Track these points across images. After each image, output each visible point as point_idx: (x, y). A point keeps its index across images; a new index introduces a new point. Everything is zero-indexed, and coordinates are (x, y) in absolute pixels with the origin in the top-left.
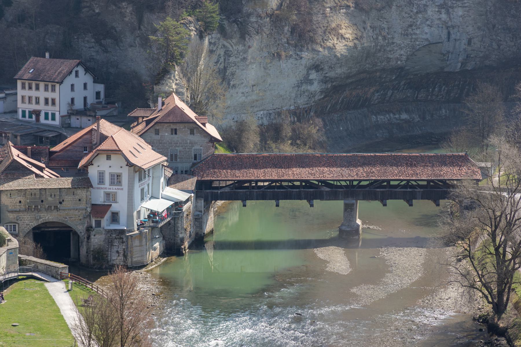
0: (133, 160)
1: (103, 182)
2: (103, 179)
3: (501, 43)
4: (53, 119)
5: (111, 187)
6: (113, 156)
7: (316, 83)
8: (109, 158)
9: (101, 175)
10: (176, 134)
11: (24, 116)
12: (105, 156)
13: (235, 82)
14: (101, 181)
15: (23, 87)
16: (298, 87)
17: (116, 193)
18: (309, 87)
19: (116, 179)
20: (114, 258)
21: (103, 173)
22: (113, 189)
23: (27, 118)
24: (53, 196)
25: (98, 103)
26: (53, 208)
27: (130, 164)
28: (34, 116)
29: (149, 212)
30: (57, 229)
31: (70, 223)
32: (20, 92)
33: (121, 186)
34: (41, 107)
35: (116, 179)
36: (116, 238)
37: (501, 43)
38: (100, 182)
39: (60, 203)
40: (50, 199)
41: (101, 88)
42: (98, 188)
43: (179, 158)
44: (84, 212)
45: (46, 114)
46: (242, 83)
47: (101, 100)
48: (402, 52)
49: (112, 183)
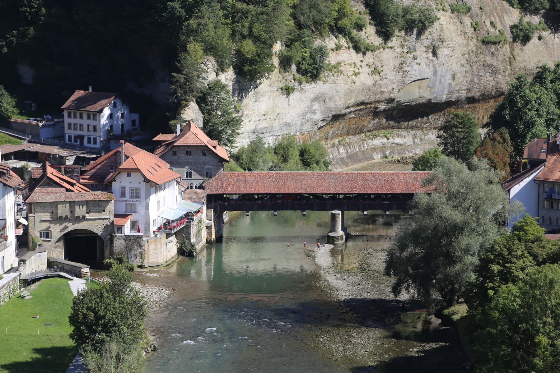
0: (149, 176)
1: (124, 196)
3: (482, 78)
4: (95, 142)
5: (131, 200)
6: (133, 174)
7: (318, 113)
8: (129, 175)
9: (123, 190)
10: (191, 154)
11: (70, 140)
12: (126, 174)
13: (248, 112)
15: (69, 116)
16: (303, 116)
17: (135, 204)
18: (312, 116)
23: (73, 142)
25: (134, 130)
27: (147, 181)
28: (78, 141)
29: (166, 220)
30: (85, 235)
32: (67, 120)
34: (85, 132)
37: (482, 78)
38: (122, 195)
41: (136, 117)
45: (89, 139)
46: (254, 113)
47: (136, 127)
48: (394, 86)
49: (132, 197)
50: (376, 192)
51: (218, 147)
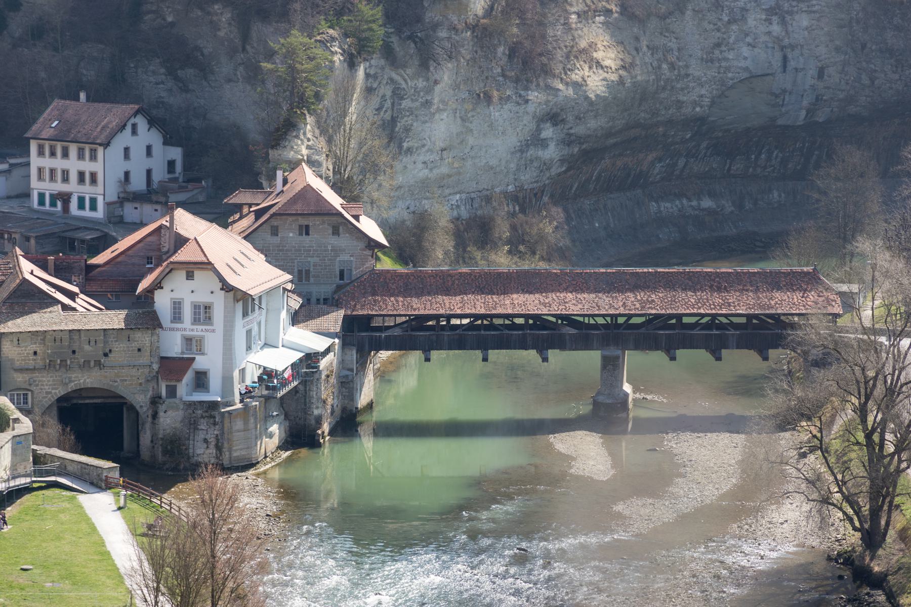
0: (232, 280)
1: (180, 318)
2: (180, 313)
4: (93, 207)
5: (195, 327)
6: (197, 274)
8: (190, 276)
9: (177, 306)
10: (307, 234)
11: (42, 202)
12: (182, 274)
13: (410, 144)
14: (177, 316)
15: (41, 153)
16: (522, 151)
18: (540, 153)
19: (203, 313)
20: (199, 451)
21: (180, 303)
22: (198, 331)
23: (48, 206)
24: (92, 343)
25: (172, 180)
26: (92, 364)
27: (227, 287)
28: (59, 204)
29: (261, 371)
30: (99, 401)
31: (122, 390)
32: (36, 162)
33: (212, 324)
34: (72, 186)
35: (203, 313)
36: (202, 417)
38: (175, 318)
39: (106, 355)
40: (87, 347)
41: (176, 153)
42: (172, 329)
43: (314, 276)
44: (147, 370)
45: (81, 200)
46: (424, 146)
47: (177, 175)
48: (703, 92)
49: (196, 321)
50: (559, 312)
51: (363, 218)
